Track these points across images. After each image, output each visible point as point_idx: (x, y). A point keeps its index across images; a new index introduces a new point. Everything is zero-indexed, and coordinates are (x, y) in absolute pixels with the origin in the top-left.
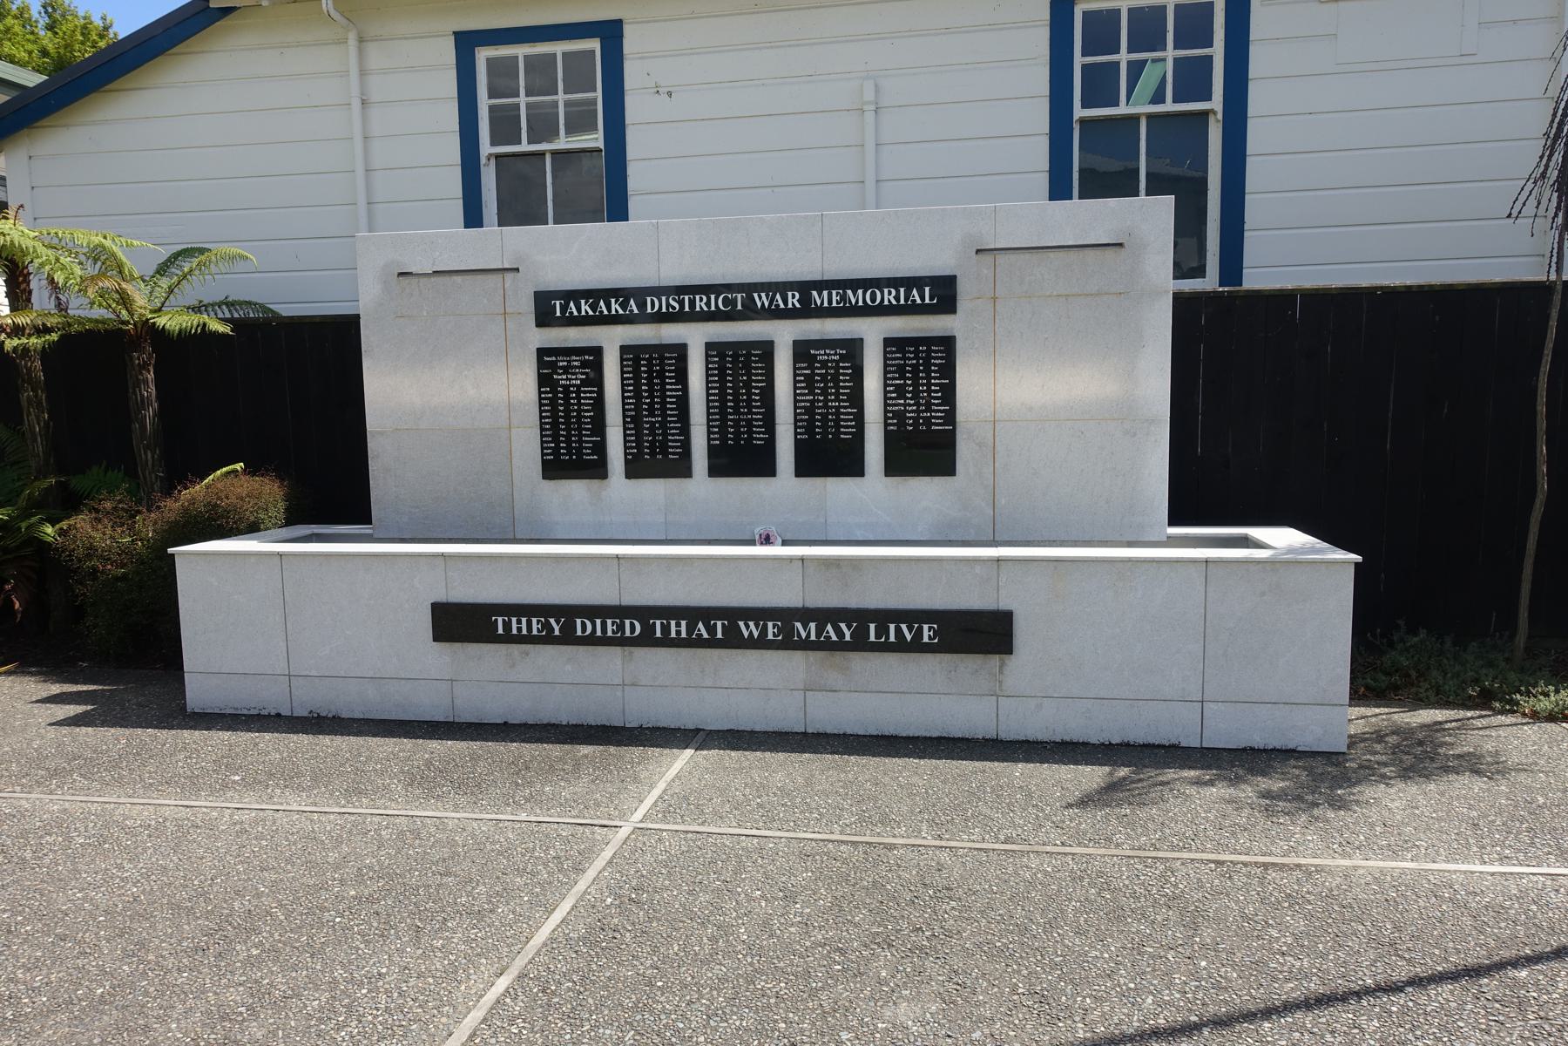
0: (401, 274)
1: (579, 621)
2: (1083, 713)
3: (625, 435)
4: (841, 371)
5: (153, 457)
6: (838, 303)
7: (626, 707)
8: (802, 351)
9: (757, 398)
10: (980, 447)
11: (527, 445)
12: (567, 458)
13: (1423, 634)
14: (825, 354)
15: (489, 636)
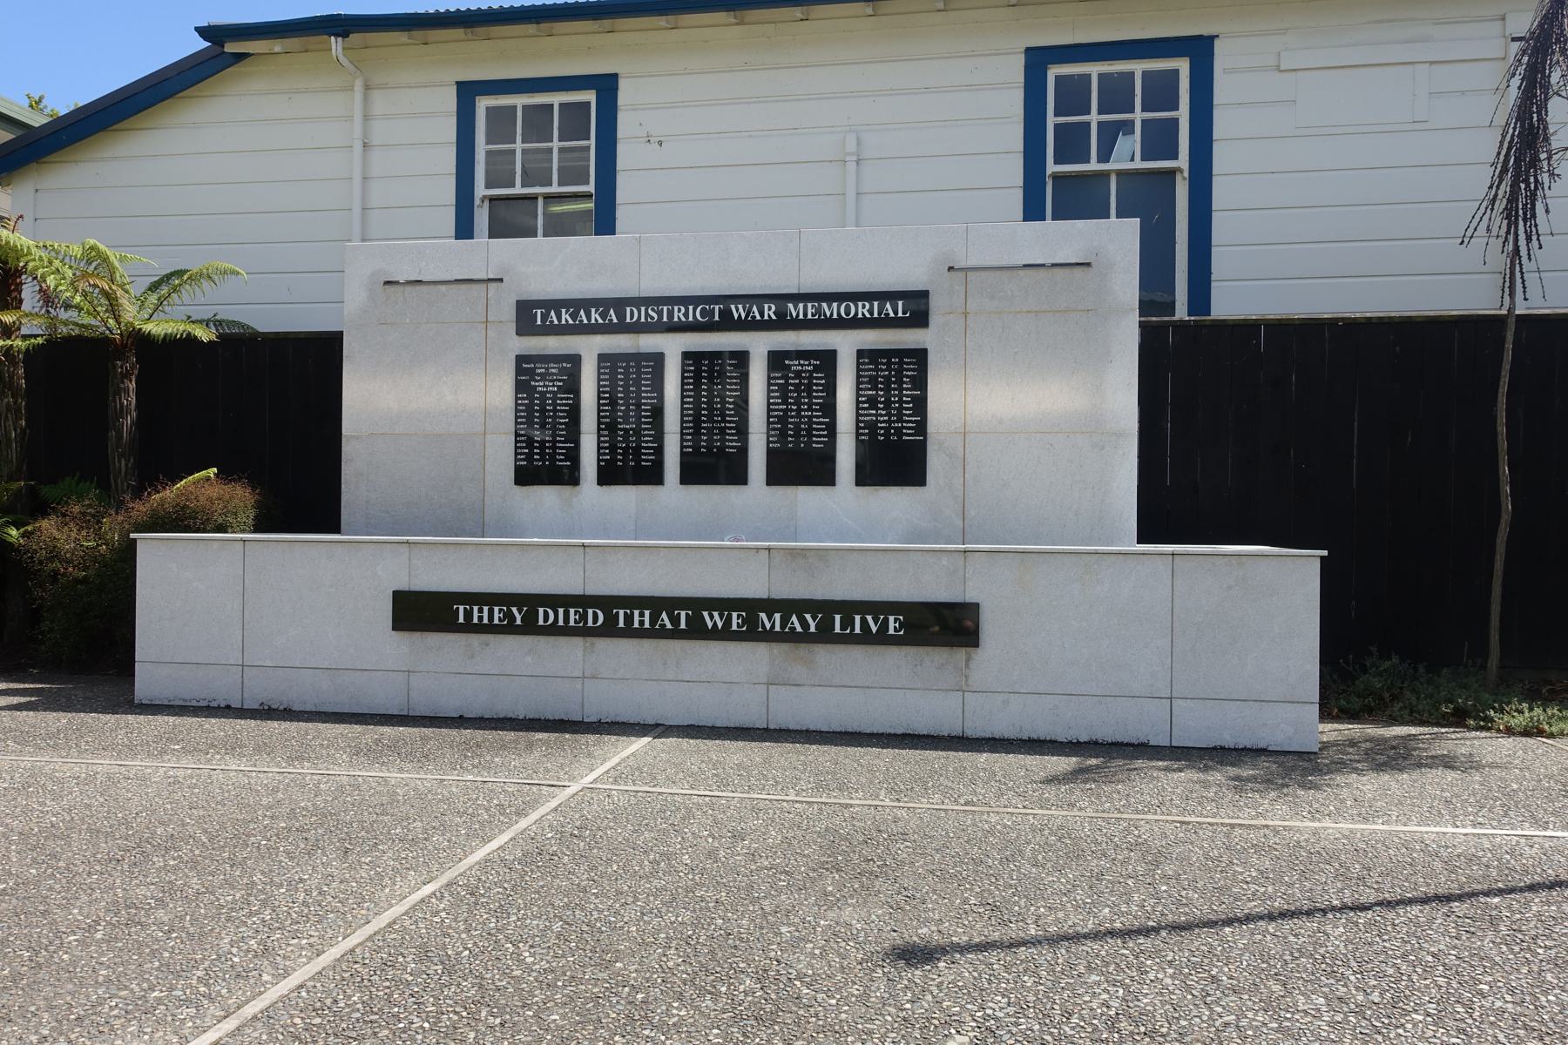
0: (951, 269)
1: (541, 610)
2: (1051, 709)
3: (599, 442)
4: (815, 381)
5: (126, 465)
6: (813, 315)
7: (585, 700)
8: (777, 360)
9: (731, 406)
10: (950, 458)
11: (501, 455)
12: (540, 463)
13: (1395, 660)
14: (799, 365)
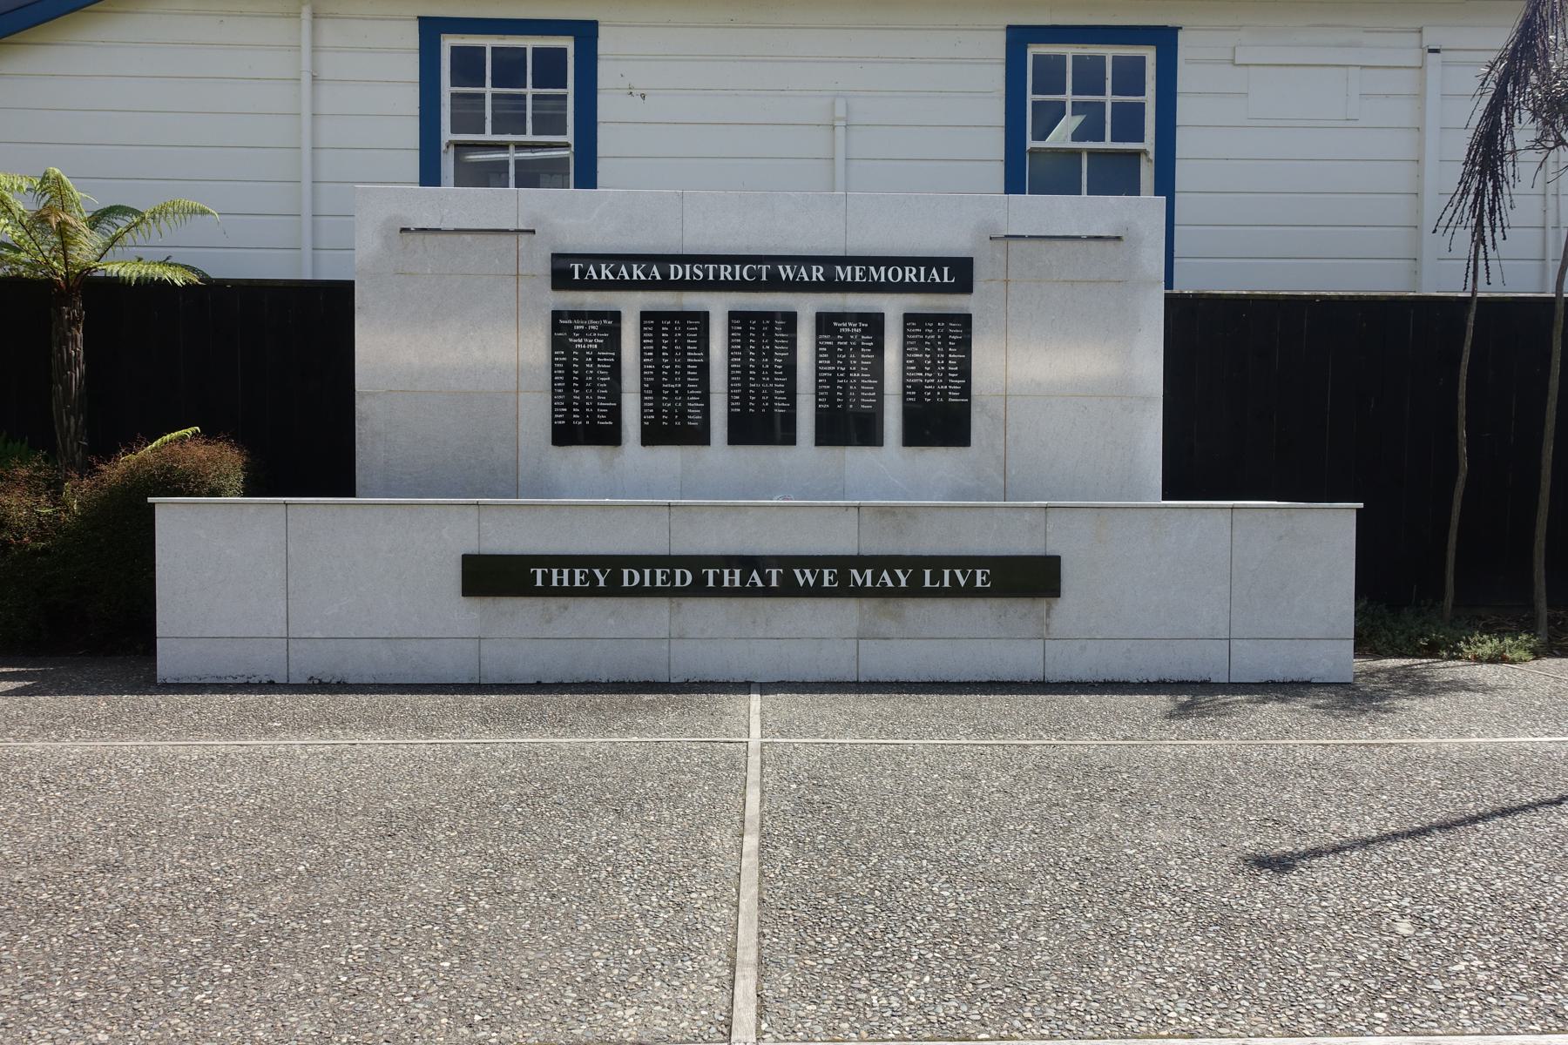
0: (403, 230)
1: (626, 572)
3: (643, 401)
4: (863, 343)
5: (76, 423)
6: (861, 278)
7: (672, 661)
8: (825, 322)
9: (780, 367)
11: (537, 411)
14: (848, 327)
15: (525, 588)
